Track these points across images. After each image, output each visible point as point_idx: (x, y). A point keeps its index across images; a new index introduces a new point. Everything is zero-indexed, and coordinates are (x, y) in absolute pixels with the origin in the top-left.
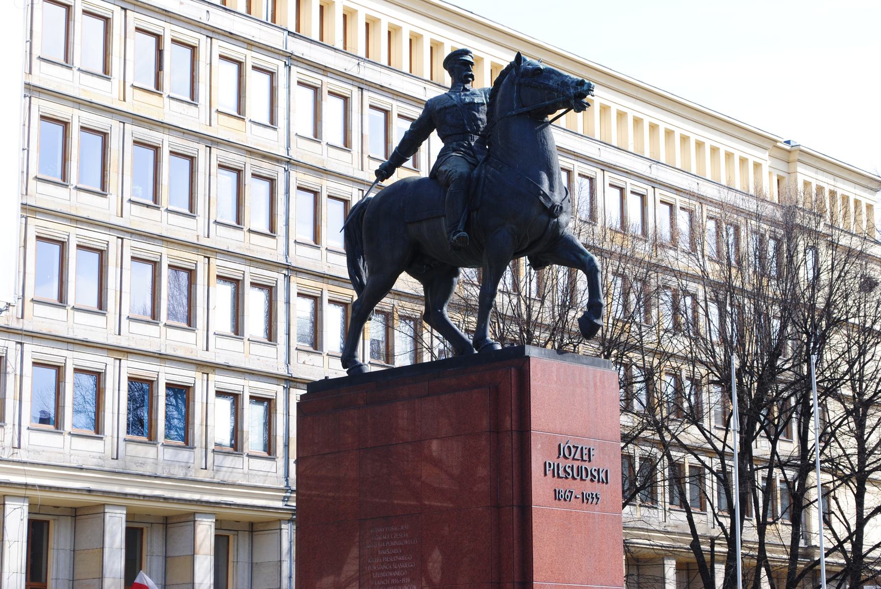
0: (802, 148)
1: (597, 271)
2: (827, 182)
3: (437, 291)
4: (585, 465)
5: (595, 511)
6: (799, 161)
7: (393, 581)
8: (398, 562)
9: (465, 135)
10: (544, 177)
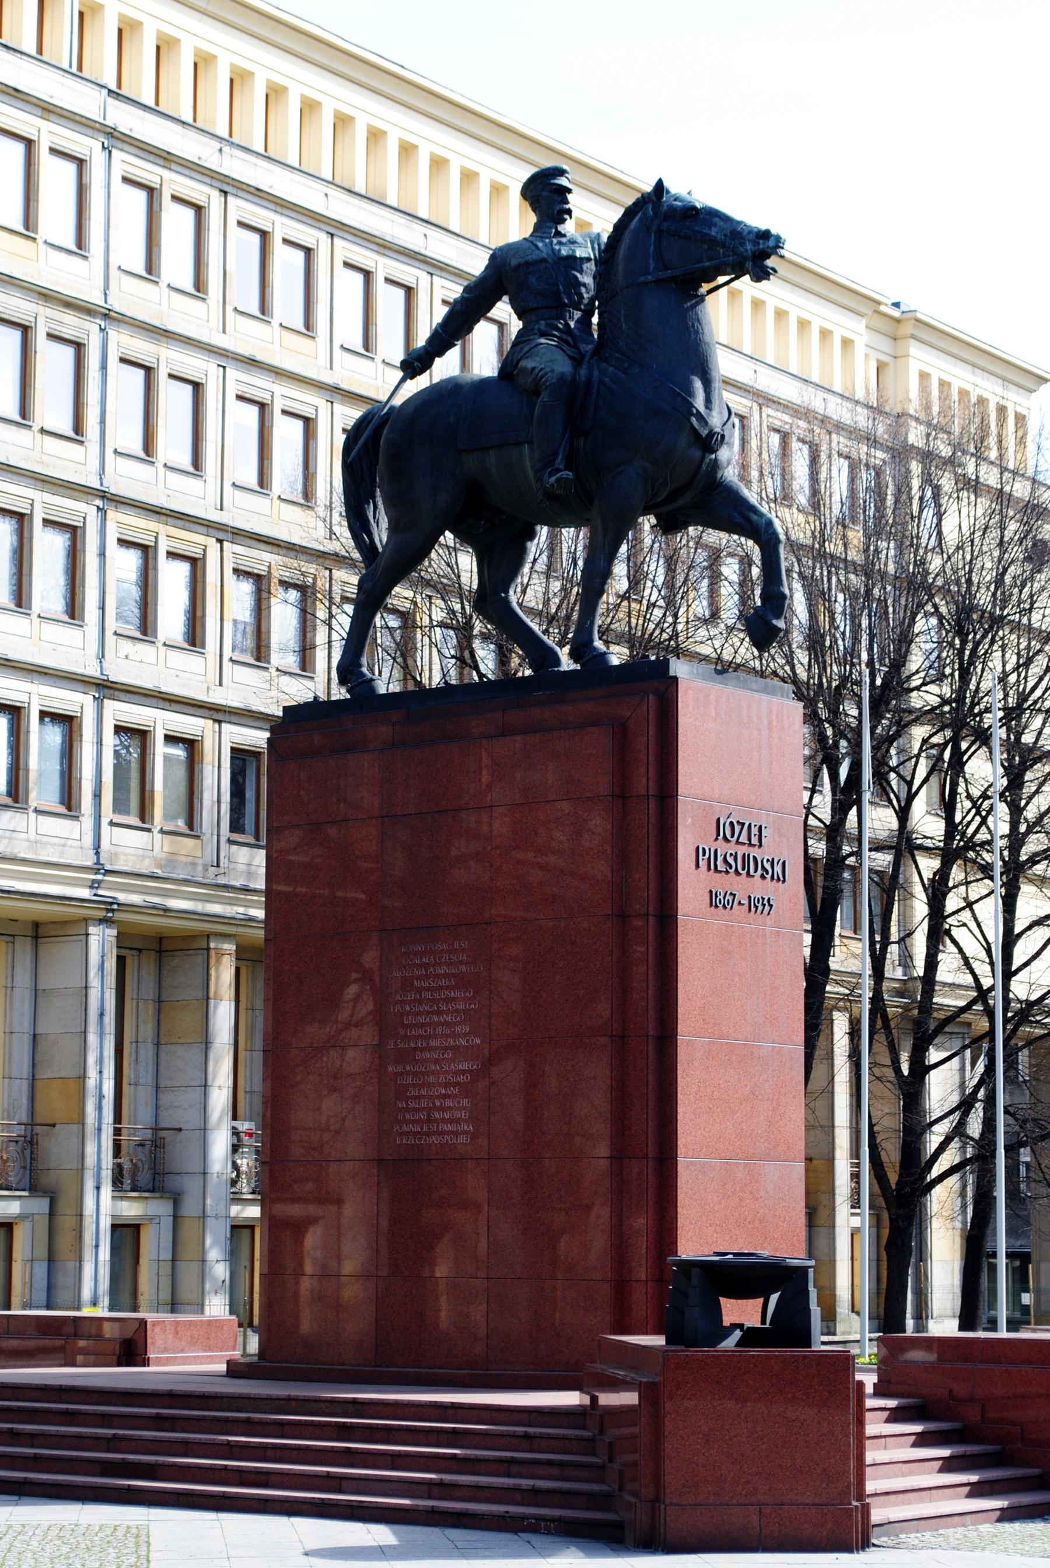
0: (919, 316)
1: (779, 541)
2: (962, 378)
3: (501, 563)
4: (754, 852)
5: (766, 924)
6: (913, 337)
7: (439, 1030)
8: (448, 1000)
9: (560, 310)
10: (698, 385)
